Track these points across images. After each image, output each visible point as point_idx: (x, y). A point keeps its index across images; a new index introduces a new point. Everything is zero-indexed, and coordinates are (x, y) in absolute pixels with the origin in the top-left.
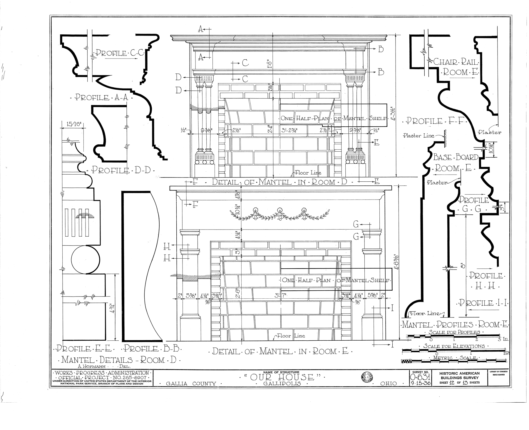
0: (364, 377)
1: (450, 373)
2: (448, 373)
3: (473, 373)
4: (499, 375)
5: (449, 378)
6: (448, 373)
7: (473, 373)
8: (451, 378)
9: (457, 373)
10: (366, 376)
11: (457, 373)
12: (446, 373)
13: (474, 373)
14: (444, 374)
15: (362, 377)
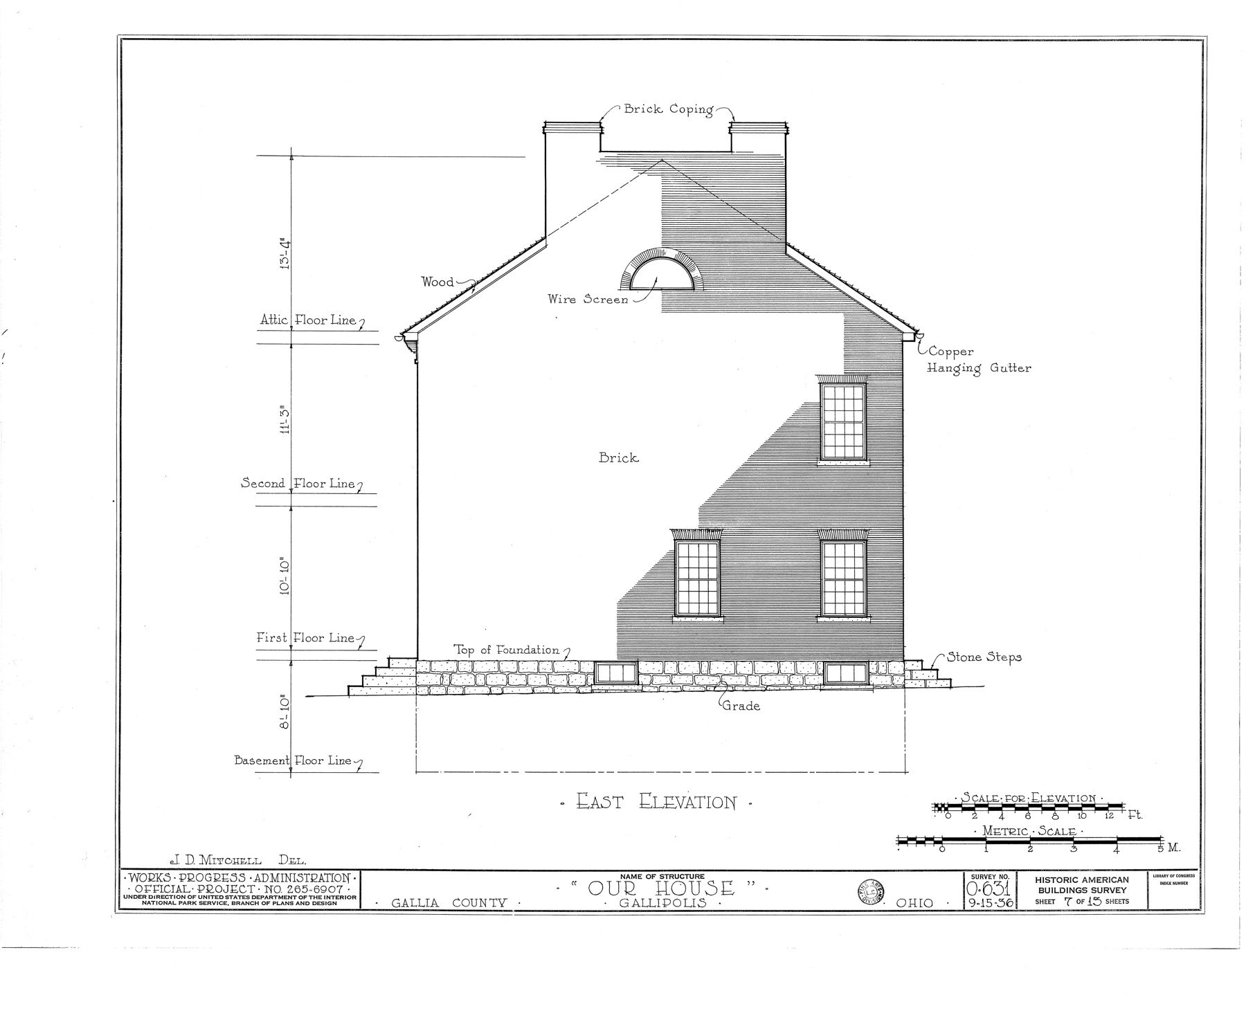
0: (862, 892)
1: (1060, 880)
2: (1055, 880)
3: (1114, 880)
5: (1058, 890)
7: (1114, 880)
8: (1063, 890)
9: (1075, 880)
10: (869, 890)
11: (1075, 880)
12: (1051, 880)
13: (1117, 880)
14: (1045, 880)
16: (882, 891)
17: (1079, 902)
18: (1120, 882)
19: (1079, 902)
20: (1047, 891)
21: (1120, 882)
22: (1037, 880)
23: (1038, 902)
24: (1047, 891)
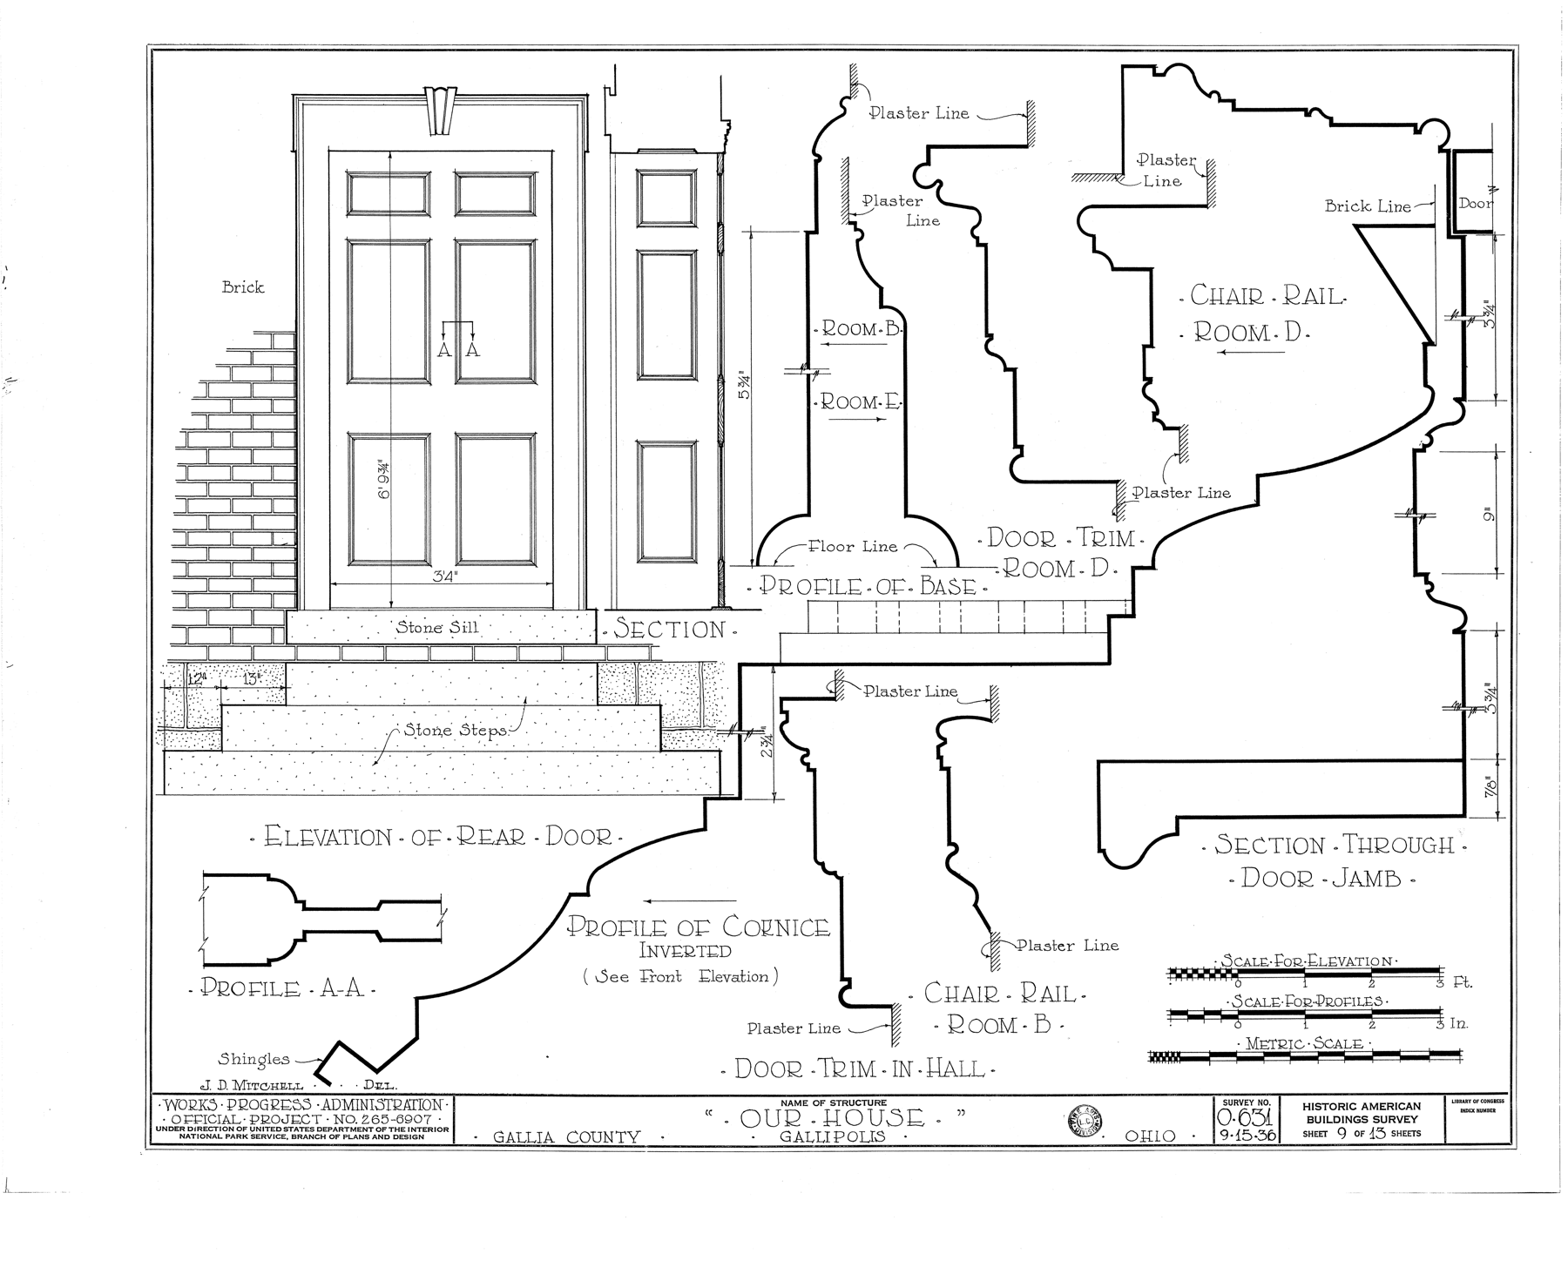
0: (1075, 1121)
1: (1333, 1107)
2: (1328, 1106)
4: (1478, 1111)
5: (1331, 1119)
6: (1328, 1106)
7: (1402, 1106)
8: (1337, 1120)
9: (1353, 1106)
10: (1083, 1118)
11: (1353, 1106)
12: (1323, 1106)
15: (1070, 1122)
16: (1099, 1119)
17: (1357, 1134)
18: (1409, 1109)
19: (1357, 1134)
20: (1318, 1120)
21: (1409, 1109)
22: (1305, 1107)
23: (1306, 1134)
24: (1318, 1120)
